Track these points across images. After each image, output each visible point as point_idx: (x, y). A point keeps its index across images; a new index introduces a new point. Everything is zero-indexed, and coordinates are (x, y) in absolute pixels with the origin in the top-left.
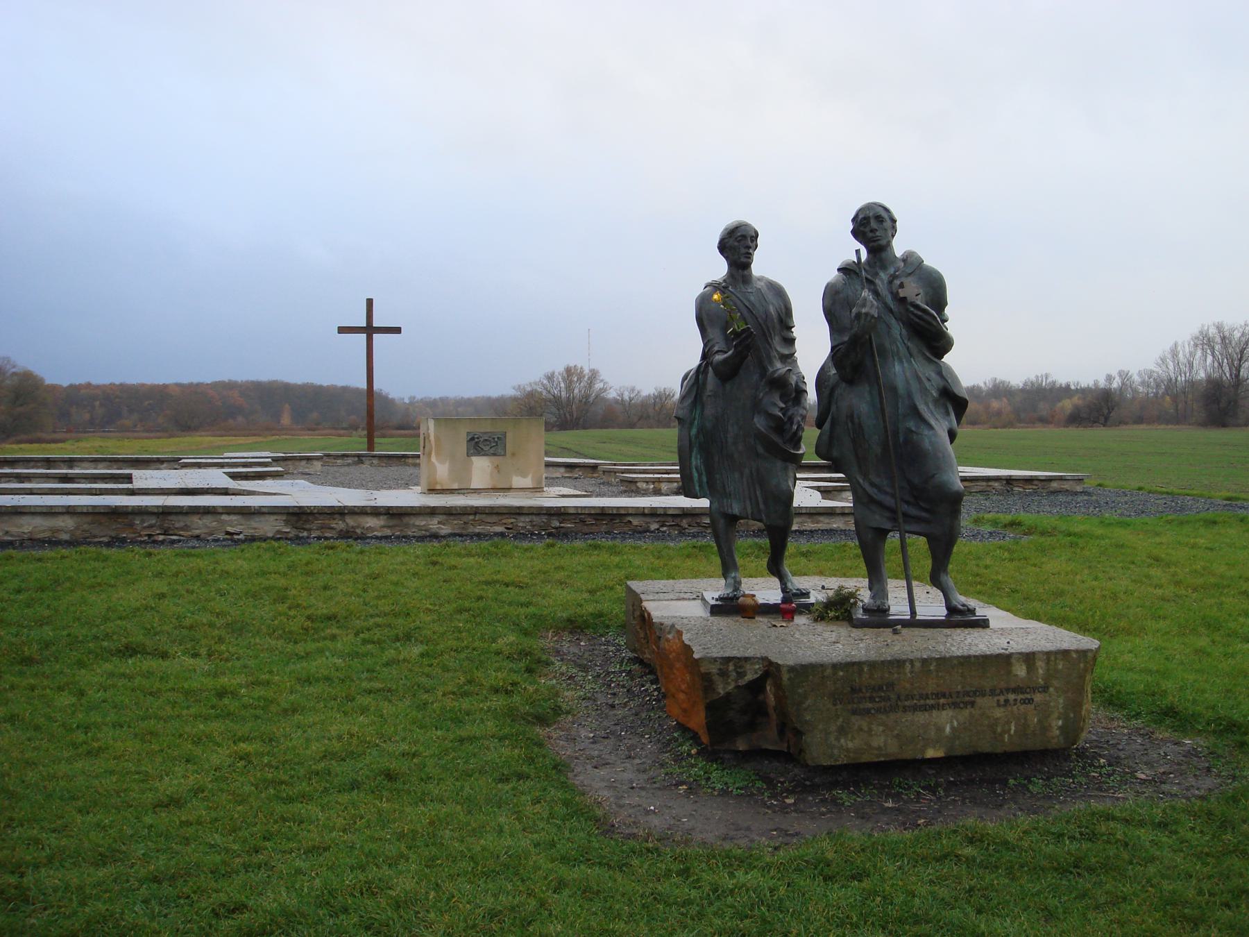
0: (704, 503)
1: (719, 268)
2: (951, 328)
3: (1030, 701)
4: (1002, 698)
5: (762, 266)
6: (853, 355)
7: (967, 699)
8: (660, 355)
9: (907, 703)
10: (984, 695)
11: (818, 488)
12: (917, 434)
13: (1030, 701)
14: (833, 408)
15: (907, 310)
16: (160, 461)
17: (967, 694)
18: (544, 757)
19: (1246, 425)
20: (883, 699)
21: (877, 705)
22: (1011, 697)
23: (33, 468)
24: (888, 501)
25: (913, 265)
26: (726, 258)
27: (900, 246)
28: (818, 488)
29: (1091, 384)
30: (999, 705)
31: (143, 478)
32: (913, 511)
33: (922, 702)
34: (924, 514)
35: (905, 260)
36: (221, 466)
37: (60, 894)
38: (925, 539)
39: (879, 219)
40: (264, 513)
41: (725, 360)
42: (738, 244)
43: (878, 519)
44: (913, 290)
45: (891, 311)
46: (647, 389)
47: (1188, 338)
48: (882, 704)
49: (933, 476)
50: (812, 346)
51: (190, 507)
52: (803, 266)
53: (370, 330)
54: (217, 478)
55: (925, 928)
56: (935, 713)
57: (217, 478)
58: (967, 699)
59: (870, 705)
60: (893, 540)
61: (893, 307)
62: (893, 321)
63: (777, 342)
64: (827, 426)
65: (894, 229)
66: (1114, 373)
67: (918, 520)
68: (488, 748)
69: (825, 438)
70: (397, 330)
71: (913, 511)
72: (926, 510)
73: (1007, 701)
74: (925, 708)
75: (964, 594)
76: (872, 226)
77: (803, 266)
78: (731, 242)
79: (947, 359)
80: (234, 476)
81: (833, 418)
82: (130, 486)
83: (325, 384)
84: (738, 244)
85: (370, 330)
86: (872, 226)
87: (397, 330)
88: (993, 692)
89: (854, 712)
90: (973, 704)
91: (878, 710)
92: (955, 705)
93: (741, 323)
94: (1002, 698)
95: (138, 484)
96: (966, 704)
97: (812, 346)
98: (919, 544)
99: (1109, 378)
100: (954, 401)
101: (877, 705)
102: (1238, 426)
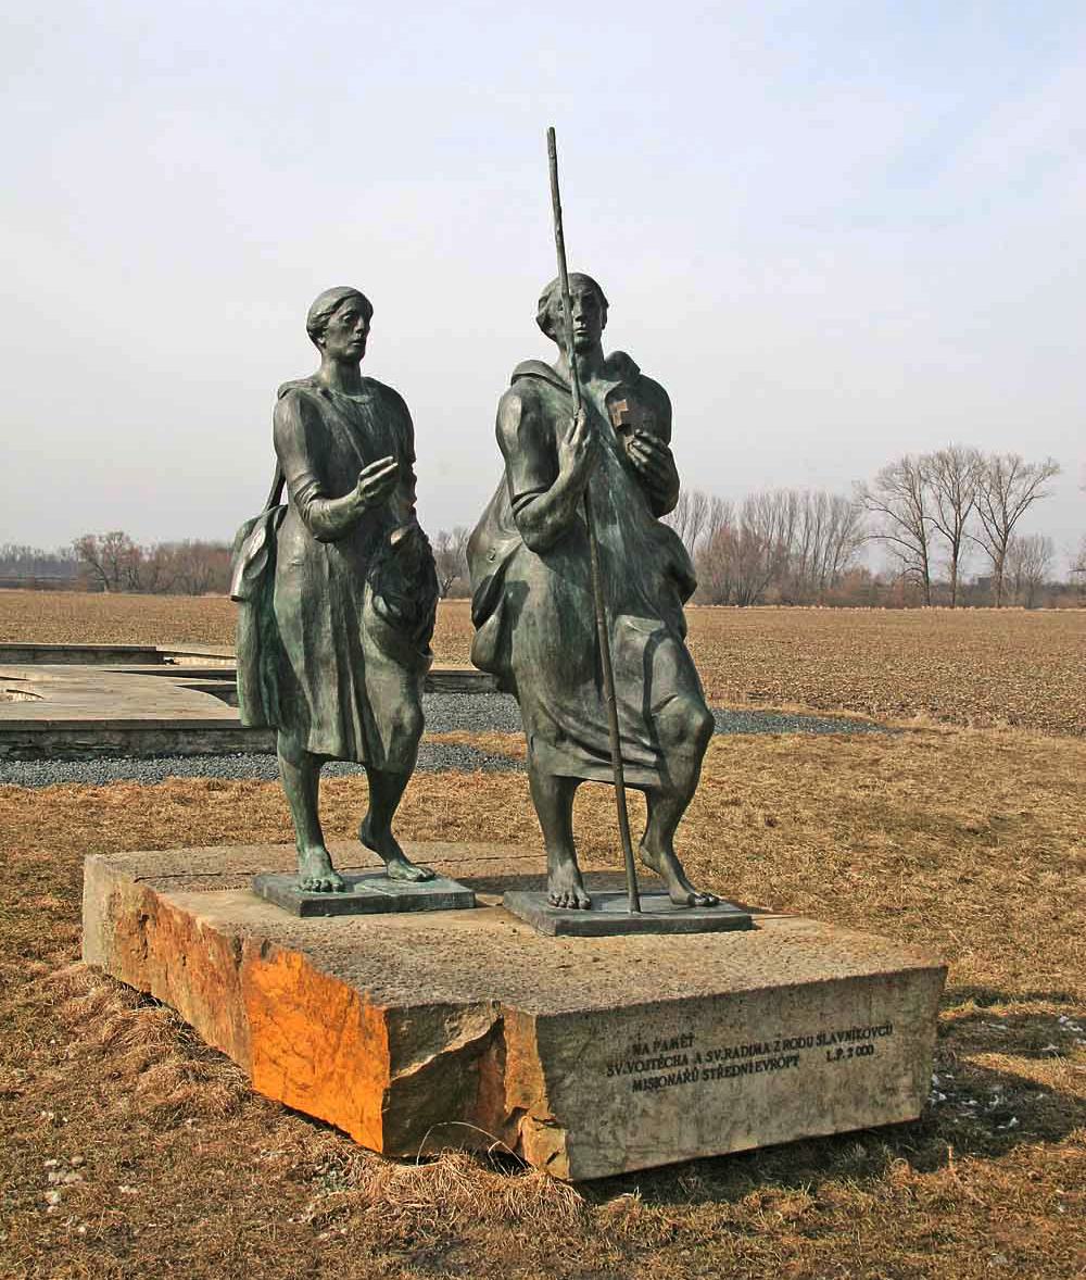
1: (310, 364)
42: (345, 321)
64: (493, 619)
73: (840, 1051)
84: (345, 321)
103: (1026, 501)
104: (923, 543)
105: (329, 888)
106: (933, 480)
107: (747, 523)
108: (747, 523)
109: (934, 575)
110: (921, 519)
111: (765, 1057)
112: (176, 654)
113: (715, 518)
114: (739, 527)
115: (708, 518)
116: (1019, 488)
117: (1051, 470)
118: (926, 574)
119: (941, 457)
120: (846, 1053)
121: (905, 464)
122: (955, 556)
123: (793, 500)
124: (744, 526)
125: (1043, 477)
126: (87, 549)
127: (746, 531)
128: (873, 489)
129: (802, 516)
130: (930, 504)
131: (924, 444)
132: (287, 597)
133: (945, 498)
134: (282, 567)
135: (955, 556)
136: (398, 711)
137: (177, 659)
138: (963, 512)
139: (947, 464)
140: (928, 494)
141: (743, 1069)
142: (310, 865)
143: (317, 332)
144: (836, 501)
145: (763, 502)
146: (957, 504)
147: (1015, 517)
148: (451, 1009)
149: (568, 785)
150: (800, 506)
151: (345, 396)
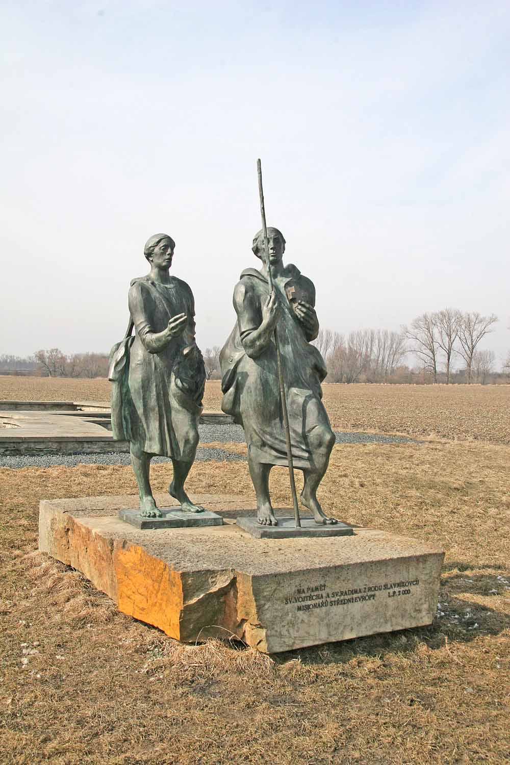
1: (146, 270)
3: (408, 592)
7: (370, 593)
9: (333, 599)
10: (380, 590)
13: (408, 592)
17: (370, 589)
18: (152, 701)
20: (318, 597)
22: (397, 589)
33: (342, 597)
37: (7, 472)
40: (115, 351)
42: (163, 249)
56: (350, 605)
58: (370, 593)
64: (232, 390)
66: (211, 348)
73: (394, 592)
74: (343, 602)
75: (180, 455)
79: (301, 274)
84: (163, 249)
88: (386, 587)
89: (299, 609)
91: (315, 606)
93: (165, 303)
94: (391, 591)
102: (257, 363)
103: (482, 334)
104: (433, 352)
105: (154, 516)
106: (439, 324)
107: (351, 344)
108: (351, 344)
109: (438, 369)
110: (432, 342)
111: (360, 595)
112: (83, 406)
113: (336, 342)
114: (347, 346)
115: (333, 342)
116: (479, 328)
117: (493, 320)
118: (435, 368)
119: (442, 313)
120: (397, 593)
121: (425, 317)
122: (449, 360)
123: (372, 334)
124: (350, 346)
125: (490, 323)
126: (41, 357)
127: (350, 348)
128: (410, 329)
129: (377, 341)
130: (437, 336)
131: (433, 308)
132: (135, 379)
133: (444, 332)
134: (133, 365)
135: (449, 360)
136: (187, 433)
137: (83, 408)
138: (452, 339)
139: (445, 317)
140: (436, 331)
141: (349, 601)
142: (146, 505)
143: (148, 255)
144: (393, 334)
145: (358, 335)
146: (449, 336)
147: (477, 342)
148: (212, 573)
149: (267, 467)
150: (376, 336)
151: (162, 285)
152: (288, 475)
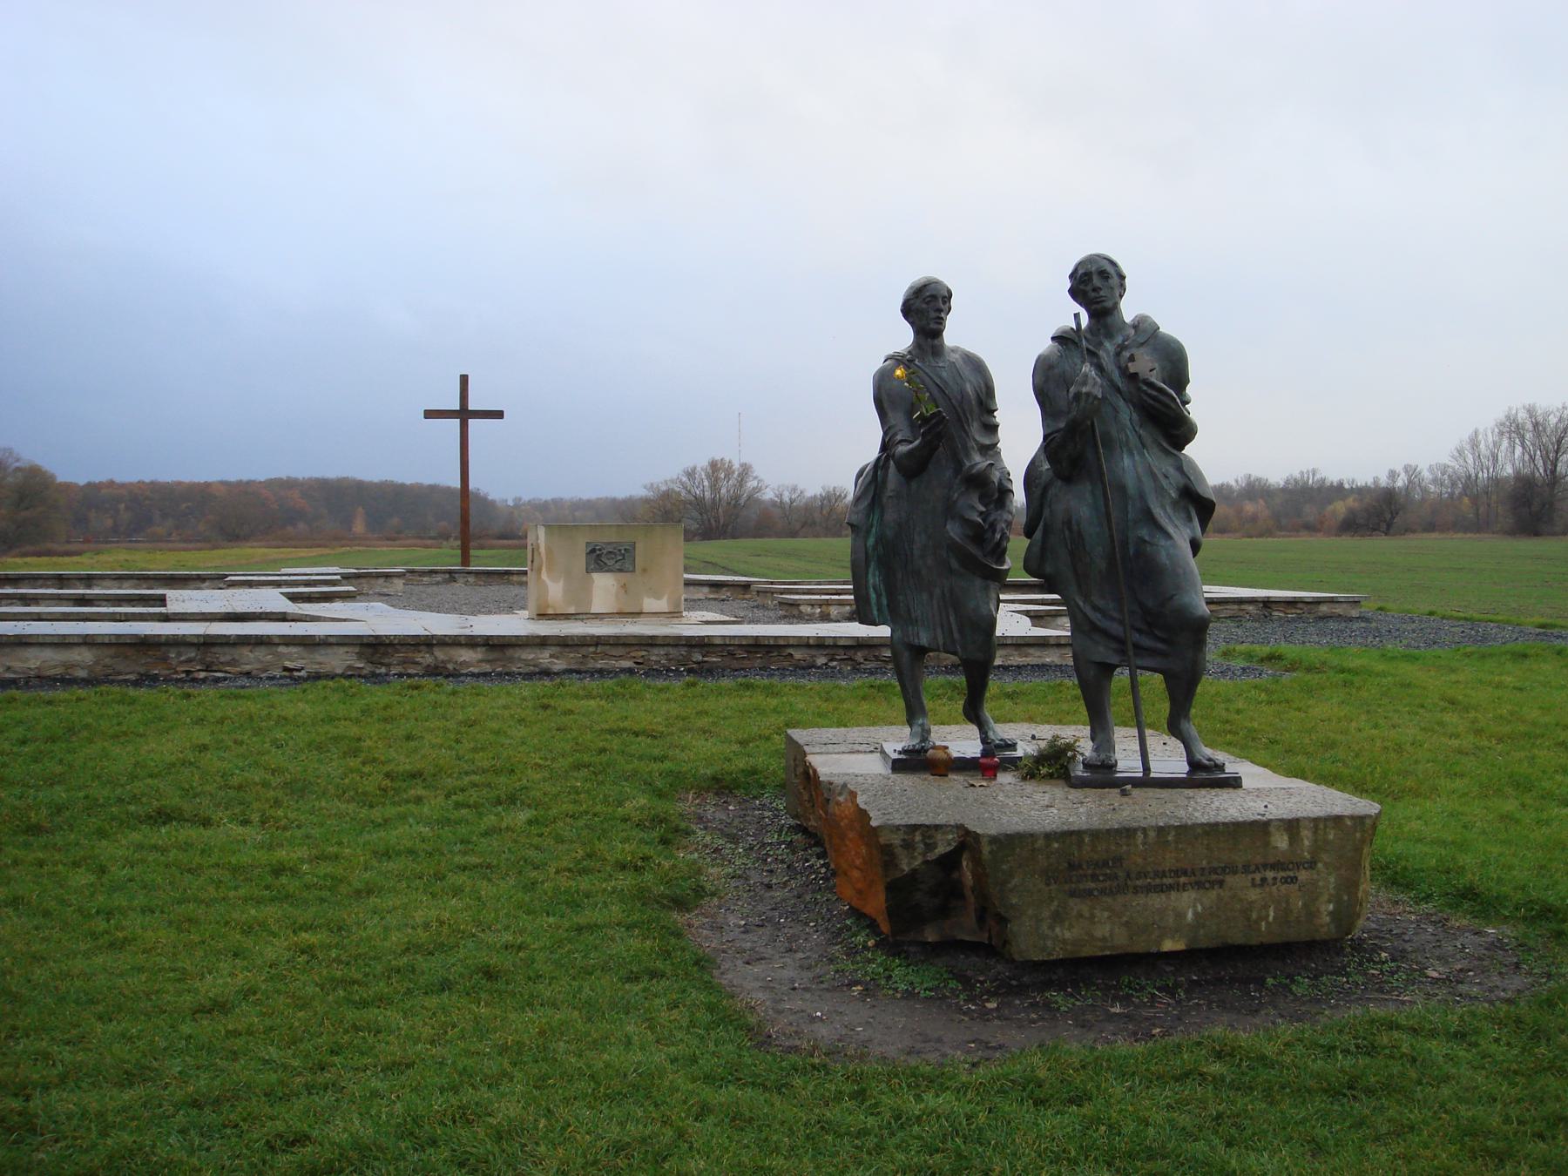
0: (884, 631)
1: (903, 337)
2: (1194, 411)
3: (1294, 880)
4: (1258, 877)
5: (956, 334)
6: (1071, 445)
7: (1214, 877)
8: (828, 445)
9: (1138, 883)
10: (1235, 873)
11: (1027, 613)
12: (1151, 544)
13: (1294, 880)
14: (1046, 512)
15: (1139, 389)
16: (201, 579)
17: (1214, 871)
19: (1564, 534)
20: (1108, 877)
21: (1101, 885)
22: (1270, 874)
23: (41, 587)
24: (1115, 628)
25: (1146, 332)
26: (912, 324)
27: (1129, 309)
28: (1027, 613)
29: (1370, 482)
30: (1254, 885)
31: (180, 600)
32: (1146, 642)
33: (1158, 881)
34: (1160, 646)
35: (1136, 326)
36: (278, 584)
37: (75, 1122)
38: (1161, 676)
39: (1104, 275)
40: (331, 644)
41: (910, 452)
42: (926, 307)
43: (1102, 652)
44: (1146, 364)
45: (1118, 390)
46: (813, 488)
47: (1491, 424)
48: (1108, 884)
49: (1171, 598)
50: (1020, 435)
51: (239, 636)
52: (1009, 334)
53: (464, 414)
54: (273, 600)
55: (1161, 1165)
56: (1173, 894)
57: (273, 600)
58: (1214, 877)
59: (1093, 885)
60: (1121, 677)
61: (1121, 385)
62: (1122, 403)
63: (975, 430)
64: (1038, 534)
65: (1123, 287)
66: (1399, 468)
67: (1153, 652)
68: (613, 939)
69: (1036, 549)
70: (498, 415)
71: (1146, 642)
72: (1163, 641)
73: (1264, 880)
74: (1161, 889)
76: (1095, 283)
77: (1009, 334)
78: (918, 304)
79: (1189, 450)
80: (294, 598)
81: (1045, 525)
82: (163, 610)
83: (408, 482)
84: (926, 307)
85: (464, 414)
86: (1095, 283)
87: (498, 415)
88: (1246, 869)
89: (1072, 894)
90: (1221, 883)
91: (1103, 892)
92: (1199, 885)
93: (930, 405)
94: (1258, 877)
95: (173, 607)
96: (1212, 883)
97: (1020, 435)
98: (1153, 683)
99: (1393, 475)
100: (1197, 503)
101: (1101, 885)
102: (1554, 534)
152: (1076, 698)
